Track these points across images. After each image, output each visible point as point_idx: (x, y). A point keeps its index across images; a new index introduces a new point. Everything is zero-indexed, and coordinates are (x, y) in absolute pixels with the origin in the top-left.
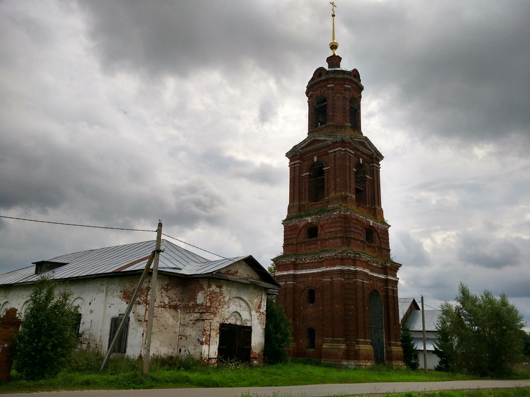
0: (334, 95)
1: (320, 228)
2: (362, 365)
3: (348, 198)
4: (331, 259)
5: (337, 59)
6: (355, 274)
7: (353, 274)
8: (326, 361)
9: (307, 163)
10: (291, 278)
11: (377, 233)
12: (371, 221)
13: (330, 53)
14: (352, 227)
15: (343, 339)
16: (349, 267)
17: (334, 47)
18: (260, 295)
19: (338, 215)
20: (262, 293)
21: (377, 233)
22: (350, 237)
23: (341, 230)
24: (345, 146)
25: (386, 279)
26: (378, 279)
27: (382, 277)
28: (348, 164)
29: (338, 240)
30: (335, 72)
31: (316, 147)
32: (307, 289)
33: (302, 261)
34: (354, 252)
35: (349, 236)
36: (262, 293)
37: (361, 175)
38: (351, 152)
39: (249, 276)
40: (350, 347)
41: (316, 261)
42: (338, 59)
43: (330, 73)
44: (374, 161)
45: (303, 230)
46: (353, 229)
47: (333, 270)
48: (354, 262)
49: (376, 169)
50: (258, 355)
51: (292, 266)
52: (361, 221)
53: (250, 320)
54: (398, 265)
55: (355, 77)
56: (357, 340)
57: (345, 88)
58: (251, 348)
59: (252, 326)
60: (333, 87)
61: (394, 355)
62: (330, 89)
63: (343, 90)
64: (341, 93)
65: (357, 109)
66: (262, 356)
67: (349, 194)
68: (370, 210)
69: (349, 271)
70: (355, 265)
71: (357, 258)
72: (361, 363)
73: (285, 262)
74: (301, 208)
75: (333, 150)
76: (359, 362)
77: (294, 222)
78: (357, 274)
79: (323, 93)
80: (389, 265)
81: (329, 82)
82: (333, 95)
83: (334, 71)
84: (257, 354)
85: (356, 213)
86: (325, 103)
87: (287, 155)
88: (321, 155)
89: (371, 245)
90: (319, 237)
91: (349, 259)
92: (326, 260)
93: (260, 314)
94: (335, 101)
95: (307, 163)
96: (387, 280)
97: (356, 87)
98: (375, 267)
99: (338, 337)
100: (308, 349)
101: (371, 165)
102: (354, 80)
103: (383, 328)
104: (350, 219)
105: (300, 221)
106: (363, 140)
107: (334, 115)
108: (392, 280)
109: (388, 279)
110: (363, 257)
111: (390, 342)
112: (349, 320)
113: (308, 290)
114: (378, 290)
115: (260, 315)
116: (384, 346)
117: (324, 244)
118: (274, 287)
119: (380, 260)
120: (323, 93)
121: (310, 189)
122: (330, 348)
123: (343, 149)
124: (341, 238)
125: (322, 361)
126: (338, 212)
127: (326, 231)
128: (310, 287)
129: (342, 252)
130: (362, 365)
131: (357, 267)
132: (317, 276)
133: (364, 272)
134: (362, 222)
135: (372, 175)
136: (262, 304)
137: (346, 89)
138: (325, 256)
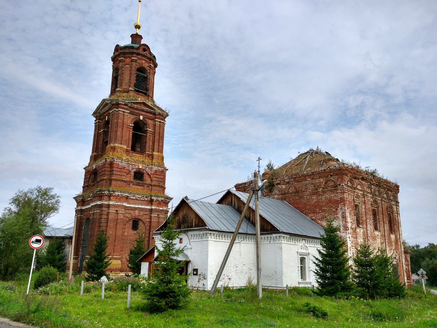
87: (94, 114)
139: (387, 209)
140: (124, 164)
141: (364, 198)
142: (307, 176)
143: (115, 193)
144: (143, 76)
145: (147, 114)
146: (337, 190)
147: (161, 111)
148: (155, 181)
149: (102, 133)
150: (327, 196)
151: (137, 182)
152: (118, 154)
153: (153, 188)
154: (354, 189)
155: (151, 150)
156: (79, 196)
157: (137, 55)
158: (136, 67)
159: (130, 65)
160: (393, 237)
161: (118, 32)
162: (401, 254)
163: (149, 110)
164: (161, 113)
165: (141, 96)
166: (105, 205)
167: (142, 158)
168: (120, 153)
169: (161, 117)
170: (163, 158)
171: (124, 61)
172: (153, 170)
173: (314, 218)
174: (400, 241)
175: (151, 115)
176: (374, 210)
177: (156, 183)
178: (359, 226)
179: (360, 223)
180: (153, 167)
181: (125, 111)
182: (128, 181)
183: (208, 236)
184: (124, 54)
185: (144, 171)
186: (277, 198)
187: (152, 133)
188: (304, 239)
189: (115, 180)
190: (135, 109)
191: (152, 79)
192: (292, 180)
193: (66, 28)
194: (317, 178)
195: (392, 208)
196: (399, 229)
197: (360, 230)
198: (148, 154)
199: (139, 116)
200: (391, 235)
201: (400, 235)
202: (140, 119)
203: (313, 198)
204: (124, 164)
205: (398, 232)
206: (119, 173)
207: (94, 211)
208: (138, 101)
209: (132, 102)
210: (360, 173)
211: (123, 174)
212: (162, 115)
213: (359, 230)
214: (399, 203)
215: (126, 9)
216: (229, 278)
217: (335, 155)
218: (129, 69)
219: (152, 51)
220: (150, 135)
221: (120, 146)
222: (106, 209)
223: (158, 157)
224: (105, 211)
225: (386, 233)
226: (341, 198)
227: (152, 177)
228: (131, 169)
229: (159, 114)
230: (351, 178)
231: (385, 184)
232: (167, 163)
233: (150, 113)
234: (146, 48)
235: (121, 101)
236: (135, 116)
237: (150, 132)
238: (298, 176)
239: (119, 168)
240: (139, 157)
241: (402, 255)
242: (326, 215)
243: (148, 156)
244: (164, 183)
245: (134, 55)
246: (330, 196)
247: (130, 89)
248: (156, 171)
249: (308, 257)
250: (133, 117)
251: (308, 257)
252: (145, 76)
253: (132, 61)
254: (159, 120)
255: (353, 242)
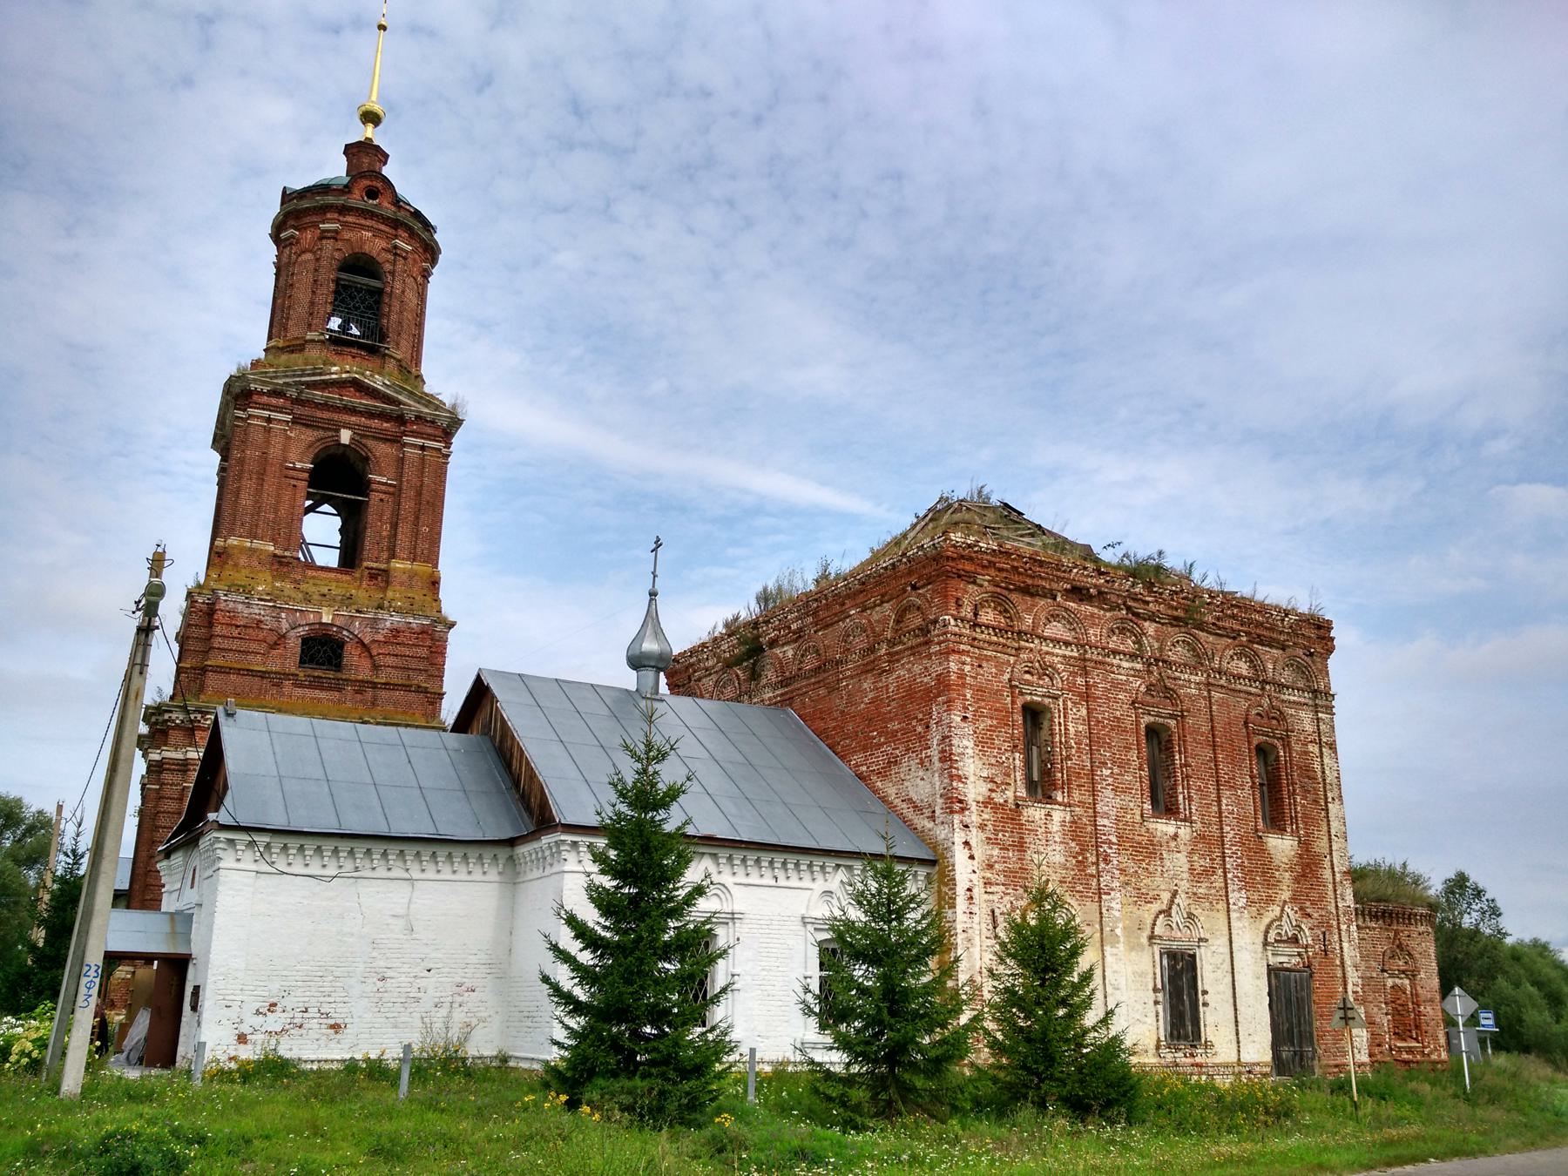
139: (1246, 723)
140: (258, 610)
141: (1086, 674)
142: (848, 596)
143: (208, 716)
144: (367, 285)
145: (368, 422)
146: (928, 643)
147: (426, 406)
148: (392, 667)
150: (902, 673)
151: (314, 677)
152: (237, 575)
153: (383, 694)
154: (1020, 639)
155: (385, 555)
157: (340, 214)
158: (337, 255)
159: (314, 253)
160: (1282, 846)
161: (731, 203)
162: (1335, 923)
163: (375, 406)
164: (427, 413)
165: (354, 357)
166: (173, 764)
167: (346, 585)
168: (245, 572)
169: (430, 431)
170: (435, 583)
171: (298, 242)
172: (381, 626)
173: (864, 768)
174: (1332, 865)
175: (385, 425)
176: (1153, 732)
177: (396, 677)
178: (1050, 797)
179: (1054, 785)
180: (383, 615)
181: (274, 415)
182: (275, 673)
183: (218, 851)
184: (297, 218)
185: (345, 633)
186: (770, 699)
187: (391, 490)
188: (846, 867)
189: (220, 670)
190: (317, 406)
191: (411, 297)
192: (810, 619)
193: (565, 210)
194: (875, 606)
195: (1284, 719)
196: (1327, 810)
197: (1049, 815)
198: (372, 569)
199: (338, 431)
200: (1264, 839)
201: (1330, 839)
202: (339, 444)
203: (865, 685)
204: (257, 611)
205: (1324, 824)
206: (235, 645)
208: (327, 377)
209: (303, 383)
210: (1059, 570)
211: (254, 646)
212: (433, 422)
213: (1043, 812)
214: (1329, 696)
215: (758, 120)
216: (332, 1022)
217: (1035, 512)
218: (311, 266)
219: (401, 190)
220: (382, 500)
221: (249, 544)
222: (176, 778)
223: (411, 578)
224: (171, 785)
225: (1227, 829)
226: (940, 675)
227: (379, 654)
228: (285, 626)
229: (417, 417)
230: (999, 590)
231: (1233, 617)
232: (451, 601)
233: (382, 416)
234: (379, 185)
235: (255, 380)
236: (321, 433)
237: (383, 488)
238: (824, 602)
239: (237, 626)
240: (334, 584)
241: (1344, 927)
242: (897, 751)
243: (373, 577)
244: (440, 677)
245: (329, 216)
246: (909, 670)
247: (308, 337)
248: (396, 632)
249: (731, 930)
250: (309, 435)
251: (731, 930)
252: (372, 284)
253: (323, 236)
254: (420, 442)
255: (997, 866)
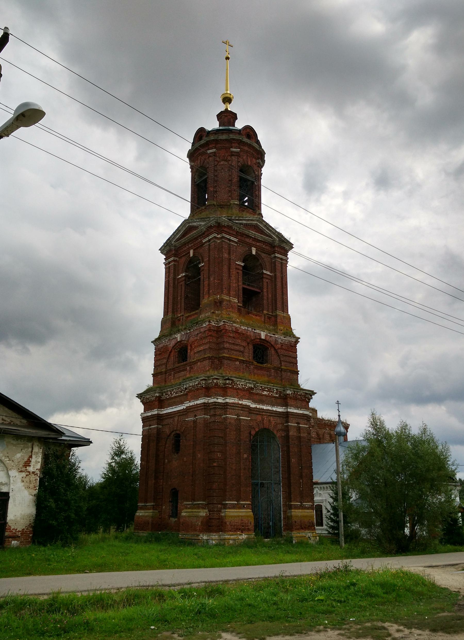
0: (216, 163)
1: (189, 348)
2: (229, 540)
3: (224, 303)
4: (196, 389)
5: (229, 115)
6: (225, 409)
7: (221, 408)
8: (184, 534)
9: (183, 259)
10: (154, 420)
11: (275, 349)
12: (262, 333)
13: (222, 107)
14: (227, 342)
15: (204, 502)
16: (215, 398)
17: (227, 100)
18: (28, 448)
19: (208, 327)
20: (33, 444)
21: (275, 349)
22: (222, 357)
23: (209, 348)
24: (221, 231)
25: (286, 412)
26: (272, 413)
27: (280, 409)
28: (226, 255)
29: (207, 362)
30: (217, 132)
31: (190, 236)
32: (173, 434)
33: (168, 396)
34: (223, 377)
35: (221, 356)
36: (33, 444)
37: (258, 271)
38: (232, 238)
39: (5, 421)
40: (213, 513)
41: (182, 394)
42: (230, 115)
43: (211, 134)
44: (275, 250)
45: (172, 353)
46: (227, 345)
47: (197, 404)
48: (224, 391)
49: (280, 262)
50: (20, 533)
51: (157, 403)
52: (244, 334)
53: (9, 483)
54: (306, 392)
55: (249, 136)
56: (223, 502)
57: (232, 152)
58: (6, 523)
59: (11, 491)
60: (215, 152)
61: (295, 522)
62: (210, 156)
63: (230, 155)
64: (226, 161)
65: (254, 181)
66: (29, 533)
67: (226, 298)
68: (269, 318)
69: (215, 405)
70: (225, 395)
71: (227, 385)
72: (226, 537)
73: (150, 399)
74: (173, 324)
75: (207, 239)
76: (224, 535)
77: (165, 342)
78: (227, 408)
79: (204, 163)
80: (290, 393)
81: (210, 146)
82: (214, 164)
83: (216, 131)
84: (19, 531)
85: (234, 322)
86: (206, 177)
87: (162, 250)
88: (197, 246)
89: (263, 366)
90: (188, 361)
91: (216, 388)
92: (191, 391)
93: (27, 473)
94: (218, 171)
95: (183, 259)
96: (288, 414)
97: (249, 150)
98: (267, 396)
99: (198, 501)
100: (171, 519)
101: (273, 256)
102: (246, 140)
103: (280, 484)
104: (223, 331)
105: (169, 340)
106: (256, 222)
107: (216, 191)
108: (296, 413)
109: (288, 412)
110: (238, 383)
111: (290, 503)
112: (212, 474)
113: (174, 435)
114: (271, 429)
115: (27, 475)
116: (282, 509)
117: (193, 369)
118: (49, 434)
119: (273, 386)
120: (204, 163)
121: (187, 296)
122: (189, 517)
123: (219, 236)
124: (209, 358)
125: (180, 535)
126: (207, 323)
127: (196, 350)
128: (176, 430)
129: (206, 378)
130: (229, 540)
131: (226, 399)
132: (183, 415)
133: (241, 404)
134: (245, 335)
135: (273, 270)
136: (33, 460)
137: (233, 153)
138: (189, 385)
149: (181, 280)
156: (148, 391)
207: (150, 426)
